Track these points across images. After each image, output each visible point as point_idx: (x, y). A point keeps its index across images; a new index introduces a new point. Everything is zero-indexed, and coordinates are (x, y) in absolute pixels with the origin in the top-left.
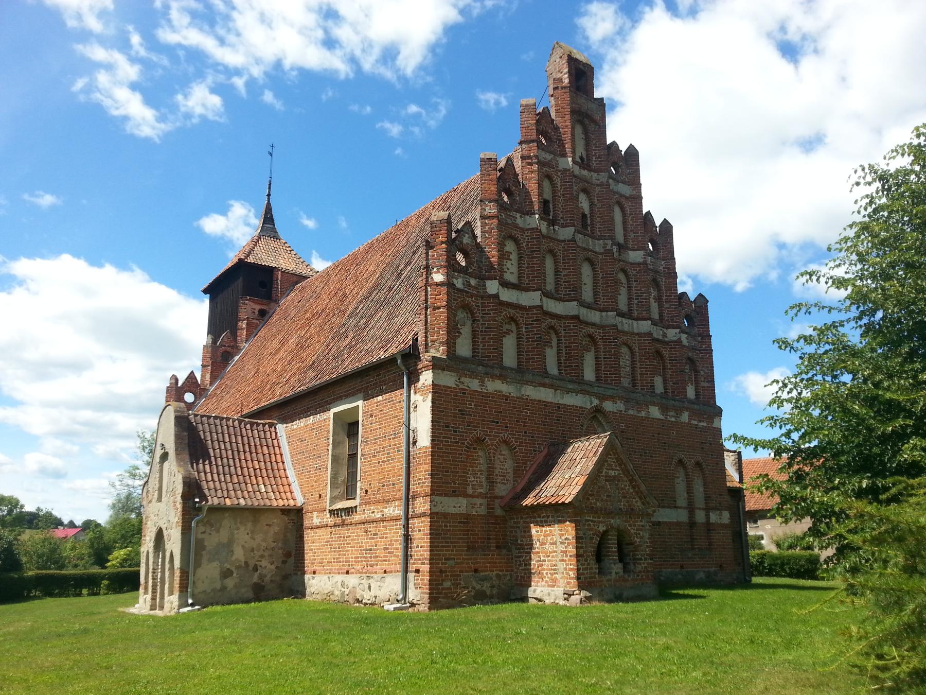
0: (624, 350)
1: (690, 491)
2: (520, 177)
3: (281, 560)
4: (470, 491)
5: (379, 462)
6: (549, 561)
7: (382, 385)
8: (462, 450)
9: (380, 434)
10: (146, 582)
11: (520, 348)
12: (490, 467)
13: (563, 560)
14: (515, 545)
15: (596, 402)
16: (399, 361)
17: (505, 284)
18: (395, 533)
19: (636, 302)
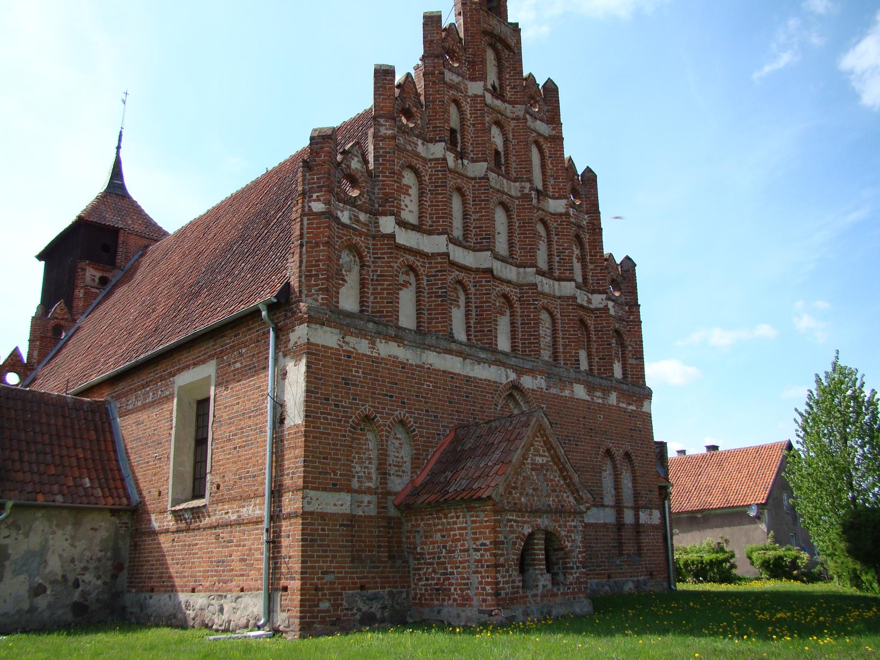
0: (544, 316)
1: (617, 487)
4: (355, 484)
6: (458, 573)
7: (241, 348)
8: (345, 431)
11: (420, 305)
12: (381, 454)
14: (413, 554)
15: (513, 376)
16: (264, 313)
18: (257, 540)
19: (557, 259)
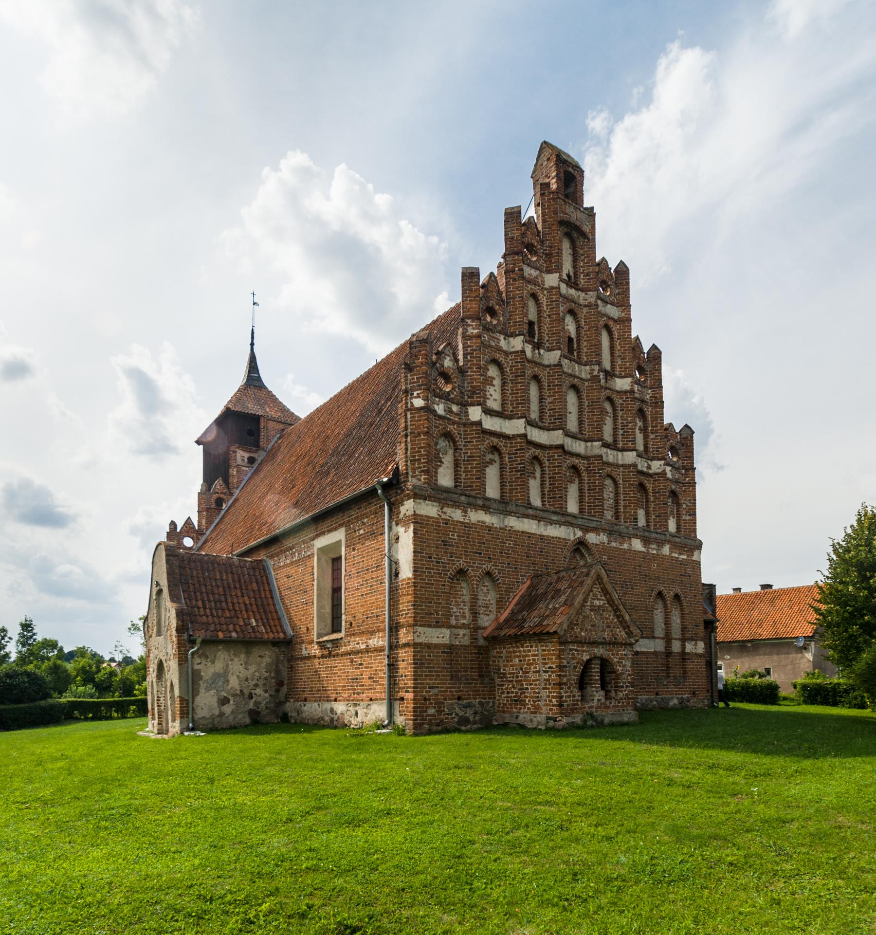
0: (608, 482)
1: (667, 623)
2: (504, 295)
3: (274, 689)
5: (362, 595)
7: (364, 518)
9: (363, 568)
10: (153, 709)
13: (546, 688)
14: (498, 673)
15: (579, 534)
16: (379, 491)
17: (488, 412)
18: (380, 663)
19: (621, 432)
